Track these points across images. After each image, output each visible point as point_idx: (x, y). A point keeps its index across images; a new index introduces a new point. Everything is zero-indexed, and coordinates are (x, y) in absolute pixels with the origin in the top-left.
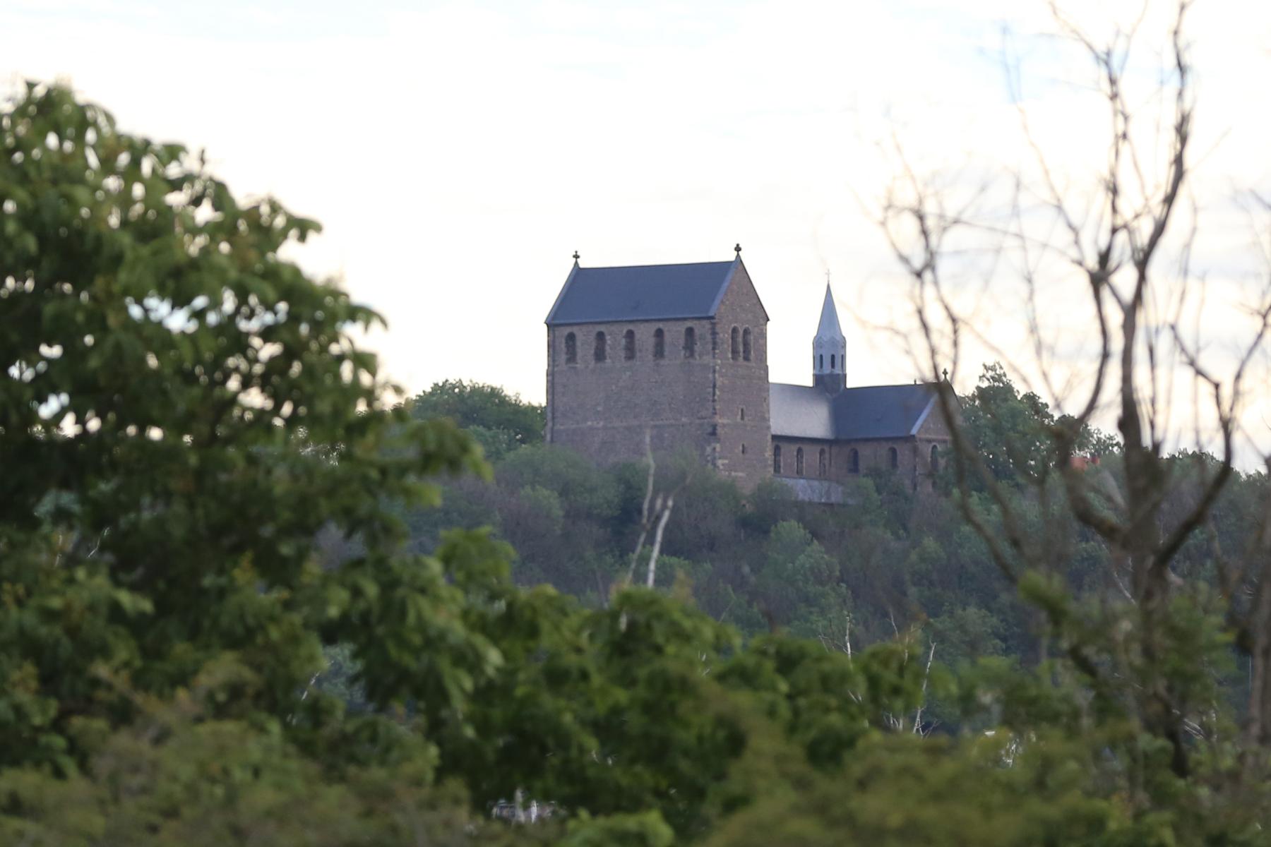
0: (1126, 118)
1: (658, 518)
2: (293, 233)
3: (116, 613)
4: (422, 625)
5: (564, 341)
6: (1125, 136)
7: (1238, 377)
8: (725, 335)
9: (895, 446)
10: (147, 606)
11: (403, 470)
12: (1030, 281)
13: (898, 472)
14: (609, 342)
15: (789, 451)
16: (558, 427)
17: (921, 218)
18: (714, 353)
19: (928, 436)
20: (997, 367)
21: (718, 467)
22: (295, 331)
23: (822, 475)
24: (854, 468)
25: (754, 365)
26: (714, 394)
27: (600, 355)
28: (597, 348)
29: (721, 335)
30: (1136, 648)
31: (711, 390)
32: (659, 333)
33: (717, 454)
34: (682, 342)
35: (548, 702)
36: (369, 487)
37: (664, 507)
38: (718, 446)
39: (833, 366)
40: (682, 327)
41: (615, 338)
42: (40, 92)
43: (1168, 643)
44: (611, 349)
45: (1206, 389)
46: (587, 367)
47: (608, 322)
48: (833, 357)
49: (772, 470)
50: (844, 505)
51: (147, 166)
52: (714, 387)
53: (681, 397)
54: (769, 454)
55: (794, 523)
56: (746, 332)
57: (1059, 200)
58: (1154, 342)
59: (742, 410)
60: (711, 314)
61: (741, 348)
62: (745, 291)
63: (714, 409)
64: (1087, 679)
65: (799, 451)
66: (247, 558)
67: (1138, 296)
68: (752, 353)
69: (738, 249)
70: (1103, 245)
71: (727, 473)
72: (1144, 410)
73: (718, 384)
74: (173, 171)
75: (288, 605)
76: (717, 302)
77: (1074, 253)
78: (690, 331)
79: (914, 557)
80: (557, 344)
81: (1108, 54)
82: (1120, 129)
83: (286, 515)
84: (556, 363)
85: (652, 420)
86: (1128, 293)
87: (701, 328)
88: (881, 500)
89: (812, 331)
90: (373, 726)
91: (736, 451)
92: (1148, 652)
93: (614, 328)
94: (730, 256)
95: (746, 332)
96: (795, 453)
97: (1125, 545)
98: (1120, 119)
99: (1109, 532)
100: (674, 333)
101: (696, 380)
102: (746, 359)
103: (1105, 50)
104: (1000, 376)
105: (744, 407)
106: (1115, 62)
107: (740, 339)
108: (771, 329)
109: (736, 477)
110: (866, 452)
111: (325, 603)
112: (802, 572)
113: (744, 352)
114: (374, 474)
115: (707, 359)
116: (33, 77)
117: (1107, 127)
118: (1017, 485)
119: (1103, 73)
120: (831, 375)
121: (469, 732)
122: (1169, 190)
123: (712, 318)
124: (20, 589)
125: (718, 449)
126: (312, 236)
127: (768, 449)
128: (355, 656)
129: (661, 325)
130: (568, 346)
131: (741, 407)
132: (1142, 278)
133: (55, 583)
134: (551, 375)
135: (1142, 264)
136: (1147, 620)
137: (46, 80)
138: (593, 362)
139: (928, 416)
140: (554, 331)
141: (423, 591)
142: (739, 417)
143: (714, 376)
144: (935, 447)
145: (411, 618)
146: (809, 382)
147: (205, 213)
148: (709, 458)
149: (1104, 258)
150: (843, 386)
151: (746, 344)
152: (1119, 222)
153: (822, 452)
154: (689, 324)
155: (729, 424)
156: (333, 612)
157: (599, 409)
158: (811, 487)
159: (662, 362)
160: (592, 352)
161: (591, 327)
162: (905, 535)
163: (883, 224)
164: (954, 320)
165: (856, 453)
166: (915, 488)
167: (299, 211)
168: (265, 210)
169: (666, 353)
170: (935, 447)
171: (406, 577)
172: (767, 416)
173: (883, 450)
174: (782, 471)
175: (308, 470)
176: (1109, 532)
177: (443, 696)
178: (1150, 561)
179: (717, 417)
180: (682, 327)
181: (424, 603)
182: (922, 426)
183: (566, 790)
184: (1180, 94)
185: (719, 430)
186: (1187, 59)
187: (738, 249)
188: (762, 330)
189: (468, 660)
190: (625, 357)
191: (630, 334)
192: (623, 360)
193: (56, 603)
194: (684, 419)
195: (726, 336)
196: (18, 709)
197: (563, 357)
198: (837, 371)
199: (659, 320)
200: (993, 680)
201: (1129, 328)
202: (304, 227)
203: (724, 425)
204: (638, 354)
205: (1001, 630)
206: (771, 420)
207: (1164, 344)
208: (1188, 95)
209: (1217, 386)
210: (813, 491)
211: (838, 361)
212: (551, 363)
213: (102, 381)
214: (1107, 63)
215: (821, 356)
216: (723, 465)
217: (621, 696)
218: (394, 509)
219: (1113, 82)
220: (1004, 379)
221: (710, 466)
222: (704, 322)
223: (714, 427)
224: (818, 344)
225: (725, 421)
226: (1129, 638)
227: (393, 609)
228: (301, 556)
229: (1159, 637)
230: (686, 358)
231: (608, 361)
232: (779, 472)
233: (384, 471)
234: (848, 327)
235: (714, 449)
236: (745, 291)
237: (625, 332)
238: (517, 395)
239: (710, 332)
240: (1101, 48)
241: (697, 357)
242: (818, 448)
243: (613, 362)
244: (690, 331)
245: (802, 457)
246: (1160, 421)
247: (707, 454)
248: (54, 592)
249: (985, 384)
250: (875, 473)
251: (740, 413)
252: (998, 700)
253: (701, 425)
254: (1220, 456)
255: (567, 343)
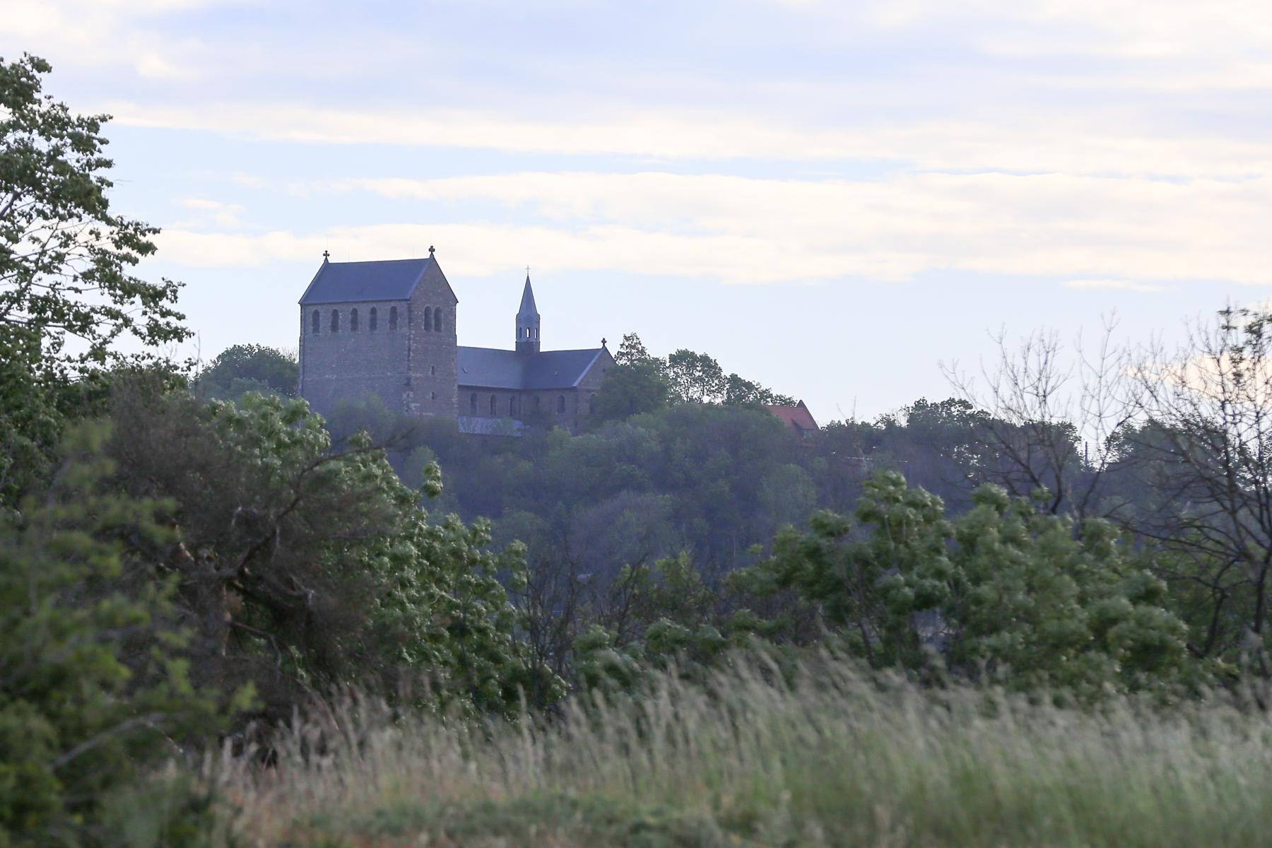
14: (341, 317)
16: (306, 379)
21: (411, 409)
26: (409, 355)
27: (334, 327)
28: (333, 322)
31: (406, 353)
32: (373, 311)
34: (388, 317)
38: (411, 394)
40: (388, 307)
46: (326, 336)
52: (409, 350)
53: (387, 358)
59: (433, 368)
61: (433, 322)
63: (409, 366)
68: (443, 325)
71: (419, 413)
73: (412, 348)
78: (394, 310)
84: (307, 332)
87: (402, 308)
94: (427, 255)
95: (438, 311)
96: (489, 400)
100: (384, 311)
105: (435, 365)
107: (432, 316)
115: (405, 330)
127: (454, 396)
129: (374, 305)
131: (432, 365)
134: (303, 341)
140: (305, 309)
142: (430, 373)
143: (409, 343)
146: (512, 347)
148: (405, 402)
154: (393, 304)
180: (388, 307)
182: (582, 380)
188: (452, 309)
190: (352, 329)
192: (350, 330)
194: (389, 374)
195: (420, 313)
197: (311, 328)
199: (373, 302)
203: (417, 379)
204: (359, 326)
212: (303, 332)
215: (521, 329)
216: (415, 407)
223: (409, 379)
224: (519, 319)
230: (391, 329)
231: (340, 331)
235: (408, 395)
238: (631, 343)
247: (403, 399)
251: (431, 369)
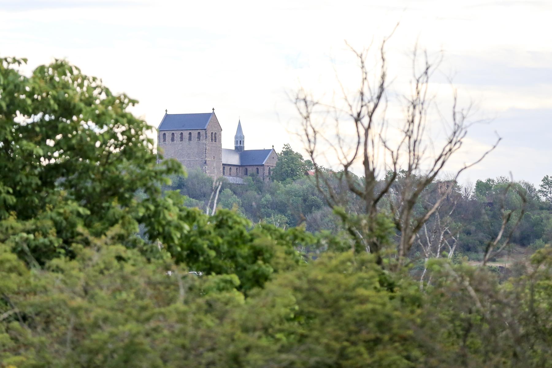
0: (366, 73)
1: (217, 188)
2: (131, 104)
3: (79, 215)
4: (165, 218)
5: (162, 135)
6: (366, 78)
7: (398, 150)
8: (209, 135)
9: (258, 168)
10: (88, 212)
11: (162, 173)
12: (337, 120)
13: (259, 175)
14: (175, 136)
15: (227, 168)
17: (306, 102)
18: (206, 140)
19: (268, 165)
20: (288, 145)
22: (130, 132)
23: (237, 176)
24: (246, 174)
25: (218, 143)
27: (173, 140)
28: (172, 138)
29: (208, 134)
30: (367, 228)
32: (190, 134)
33: (206, 169)
34: (197, 136)
35: (200, 241)
36: (151, 177)
37: (219, 184)
38: (207, 167)
39: (240, 144)
40: (197, 132)
41: (177, 135)
42: (59, 62)
43: (377, 227)
44: (176, 138)
45: (389, 153)
47: (175, 130)
48: (240, 141)
49: (222, 174)
50: (243, 184)
51: (86, 83)
52: (206, 149)
54: (221, 169)
55: (229, 190)
56: (215, 134)
57: (346, 97)
58: (374, 138)
59: (214, 156)
60: (205, 128)
61: (214, 139)
62: (215, 122)
64: (353, 237)
65: (230, 168)
66: (116, 198)
67: (369, 127)
69: (213, 109)
70: (359, 111)
72: (370, 160)
73: (207, 148)
74: (94, 85)
75: (128, 212)
76: (207, 124)
77: (350, 113)
78: (199, 133)
79: (263, 200)
80: (160, 136)
81: (361, 55)
82: (364, 76)
83: (127, 186)
84: (160, 142)
85: (188, 159)
86: (366, 125)
87: (203, 133)
88: (254, 183)
89: (234, 133)
90: (152, 247)
91: (212, 168)
92: (371, 229)
93: (177, 132)
94: (211, 111)
95: (215, 134)
96: (229, 169)
97: (365, 198)
98: (364, 74)
99: (360, 194)
100: (195, 134)
101: (201, 147)
102: (215, 141)
103: (360, 54)
104: (289, 147)
106: (363, 57)
107: (214, 136)
108: (223, 133)
109: (212, 176)
110: (249, 169)
111: (137, 212)
112: (230, 204)
113: (215, 139)
114: (153, 174)
115: (204, 141)
116: (57, 58)
117: (361, 76)
118: (293, 179)
119: (360, 60)
120: (240, 146)
121: (179, 249)
122: (379, 94)
123: (206, 129)
124: (51, 206)
125: (207, 168)
126: (136, 105)
128: (146, 226)
129: (173, 132)
130: (163, 137)
131: (213, 155)
132: (370, 120)
133: (61, 205)
135: (370, 117)
136: (371, 220)
137: (61, 58)
138: (171, 142)
139: (268, 159)
141: (166, 208)
142: (213, 158)
144: (270, 168)
145: (162, 216)
146: (233, 148)
147: (103, 96)
148: (204, 170)
149: (359, 114)
150: (243, 150)
151: (215, 137)
152: (364, 103)
153: (237, 169)
154: (199, 131)
155: (210, 160)
156: (141, 214)
157: (172, 155)
158: (233, 179)
159: (191, 142)
160: (171, 139)
161: (170, 131)
162: (261, 193)
163: (296, 103)
164: (315, 132)
165: (247, 169)
166: (264, 179)
167: (132, 97)
168: (122, 97)
169: (192, 139)
170: (270, 168)
171: (161, 204)
172: (221, 158)
173: (255, 168)
174: (225, 174)
175: (131, 173)
176: (360, 194)
177: (172, 239)
178: (372, 203)
179: (207, 158)
180: (197, 132)
181: (166, 212)
183: (205, 267)
184: (383, 67)
185: (207, 162)
186: (385, 56)
187: (213, 109)
189: (179, 228)
191: (182, 134)
193: (62, 211)
196: (51, 242)
198: (242, 145)
199: (190, 130)
200: (326, 237)
201: (366, 135)
202: (134, 102)
204: (184, 140)
205: (289, 222)
206: (222, 159)
207: (376, 140)
208: (385, 67)
209: (392, 152)
210: (234, 180)
211: (242, 142)
212: (159, 142)
213: (76, 147)
214: (361, 57)
215: (237, 141)
217: (220, 240)
218: (158, 185)
219: (362, 62)
220: (290, 148)
221: (204, 172)
222: (203, 130)
223: (206, 161)
224: (236, 137)
225: (209, 159)
226: (366, 225)
227: (156, 214)
228: (131, 197)
229: (375, 226)
230: (198, 141)
231: (175, 141)
232: (224, 174)
233: (156, 173)
234: (245, 132)
235: (206, 167)
236: (215, 122)
237: (180, 133)
239: (205, 133)
240: (359, 53)
241: (201, 141)
242: (235, 168)
243: (177, 142)
244: (199, 133)
245: (231, 170)
246: (375, 162)
247: (203, 169)
248: (61, 208)
249: (284, 150)
250: (252, 175)
252: (327, 243)
253: (202, 160)
254: (394, 171)
255: (163, 136)
